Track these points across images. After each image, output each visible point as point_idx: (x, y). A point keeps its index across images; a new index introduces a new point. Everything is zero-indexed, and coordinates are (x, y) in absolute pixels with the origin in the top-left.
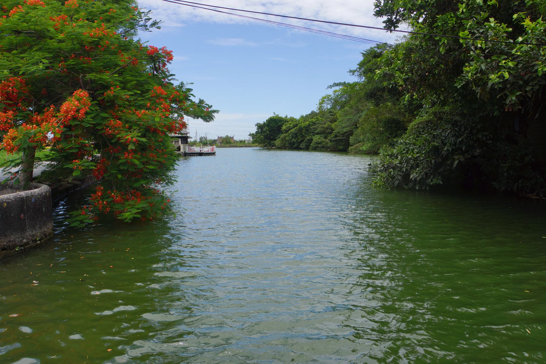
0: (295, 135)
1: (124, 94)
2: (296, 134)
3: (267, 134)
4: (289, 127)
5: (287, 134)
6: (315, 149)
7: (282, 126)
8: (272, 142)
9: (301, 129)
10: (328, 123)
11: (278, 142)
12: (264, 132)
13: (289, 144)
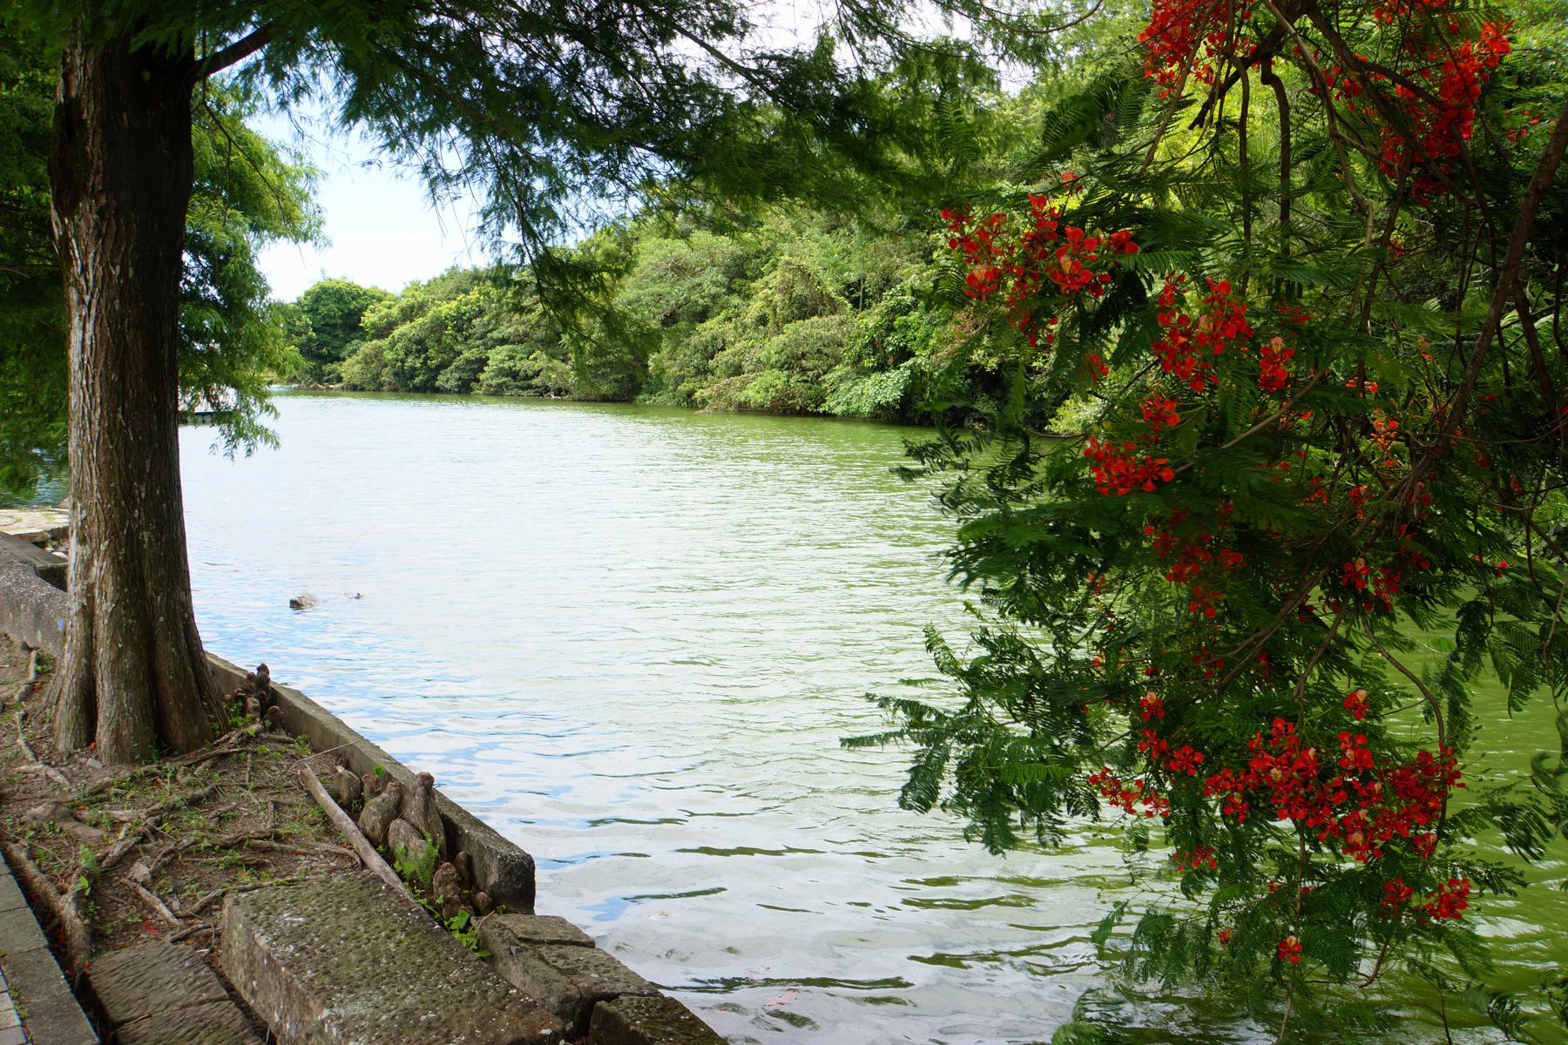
0: (419, 346)
1: (791, 883)
2: (420, 342)
3: (310, 340)
4: (388, 316)
5: (385, 343)
6: (497, 393)
7: (359, 312)
8: (327, 368)
9: (439, 325)
10: (23, 681)
11: (350, 368)
12: (299, 334)
13: (396, 374)
